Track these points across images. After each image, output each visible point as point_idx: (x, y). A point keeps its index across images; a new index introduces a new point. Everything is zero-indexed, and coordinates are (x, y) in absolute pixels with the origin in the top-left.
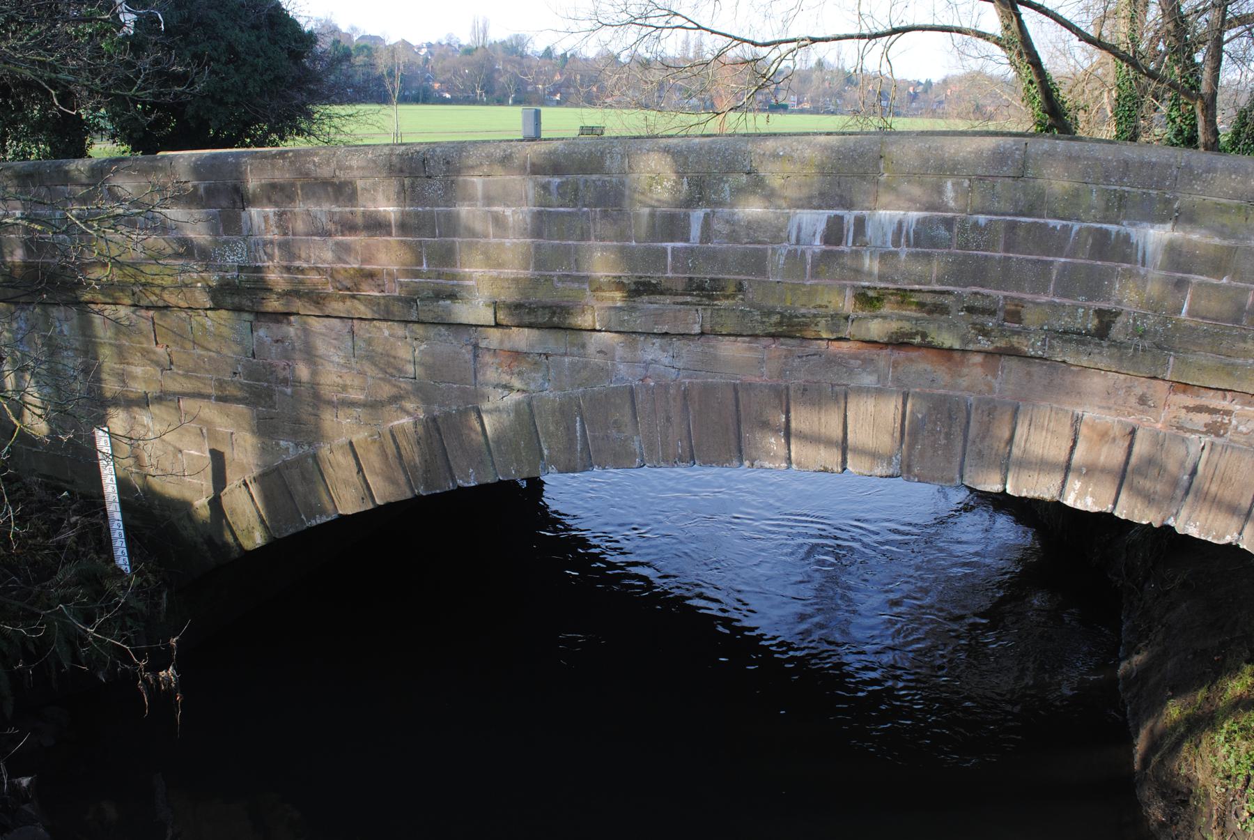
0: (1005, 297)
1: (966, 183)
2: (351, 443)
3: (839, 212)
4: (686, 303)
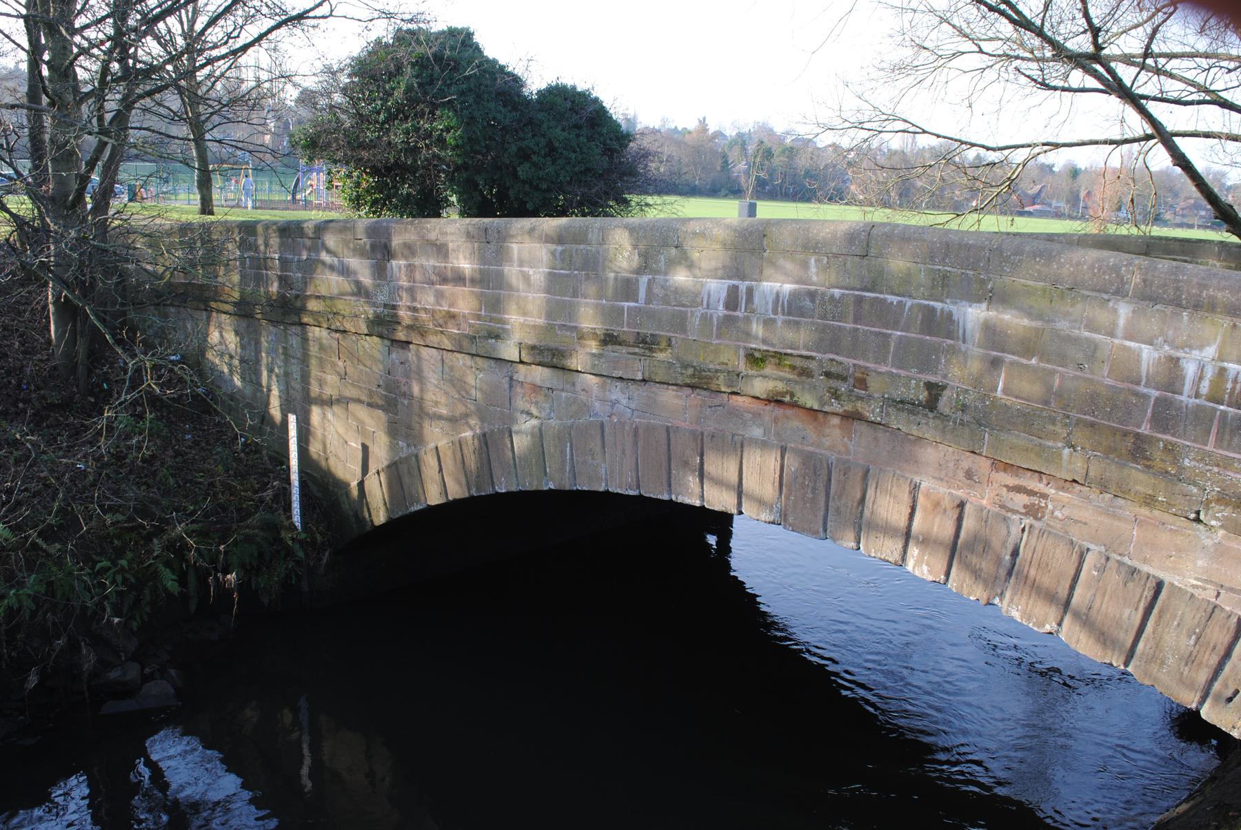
0: (854, 365)
1: (825, 261)
2: (437, 448)
3: (735, 282)
4: (635, 354)
